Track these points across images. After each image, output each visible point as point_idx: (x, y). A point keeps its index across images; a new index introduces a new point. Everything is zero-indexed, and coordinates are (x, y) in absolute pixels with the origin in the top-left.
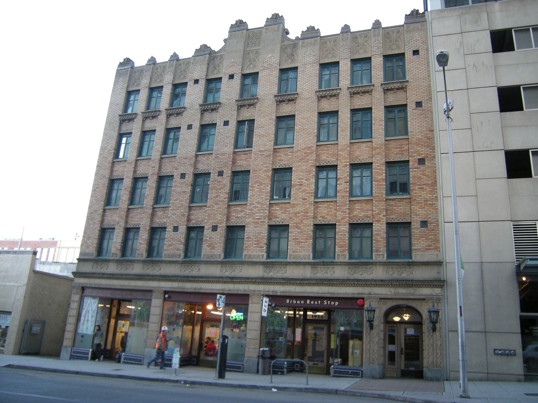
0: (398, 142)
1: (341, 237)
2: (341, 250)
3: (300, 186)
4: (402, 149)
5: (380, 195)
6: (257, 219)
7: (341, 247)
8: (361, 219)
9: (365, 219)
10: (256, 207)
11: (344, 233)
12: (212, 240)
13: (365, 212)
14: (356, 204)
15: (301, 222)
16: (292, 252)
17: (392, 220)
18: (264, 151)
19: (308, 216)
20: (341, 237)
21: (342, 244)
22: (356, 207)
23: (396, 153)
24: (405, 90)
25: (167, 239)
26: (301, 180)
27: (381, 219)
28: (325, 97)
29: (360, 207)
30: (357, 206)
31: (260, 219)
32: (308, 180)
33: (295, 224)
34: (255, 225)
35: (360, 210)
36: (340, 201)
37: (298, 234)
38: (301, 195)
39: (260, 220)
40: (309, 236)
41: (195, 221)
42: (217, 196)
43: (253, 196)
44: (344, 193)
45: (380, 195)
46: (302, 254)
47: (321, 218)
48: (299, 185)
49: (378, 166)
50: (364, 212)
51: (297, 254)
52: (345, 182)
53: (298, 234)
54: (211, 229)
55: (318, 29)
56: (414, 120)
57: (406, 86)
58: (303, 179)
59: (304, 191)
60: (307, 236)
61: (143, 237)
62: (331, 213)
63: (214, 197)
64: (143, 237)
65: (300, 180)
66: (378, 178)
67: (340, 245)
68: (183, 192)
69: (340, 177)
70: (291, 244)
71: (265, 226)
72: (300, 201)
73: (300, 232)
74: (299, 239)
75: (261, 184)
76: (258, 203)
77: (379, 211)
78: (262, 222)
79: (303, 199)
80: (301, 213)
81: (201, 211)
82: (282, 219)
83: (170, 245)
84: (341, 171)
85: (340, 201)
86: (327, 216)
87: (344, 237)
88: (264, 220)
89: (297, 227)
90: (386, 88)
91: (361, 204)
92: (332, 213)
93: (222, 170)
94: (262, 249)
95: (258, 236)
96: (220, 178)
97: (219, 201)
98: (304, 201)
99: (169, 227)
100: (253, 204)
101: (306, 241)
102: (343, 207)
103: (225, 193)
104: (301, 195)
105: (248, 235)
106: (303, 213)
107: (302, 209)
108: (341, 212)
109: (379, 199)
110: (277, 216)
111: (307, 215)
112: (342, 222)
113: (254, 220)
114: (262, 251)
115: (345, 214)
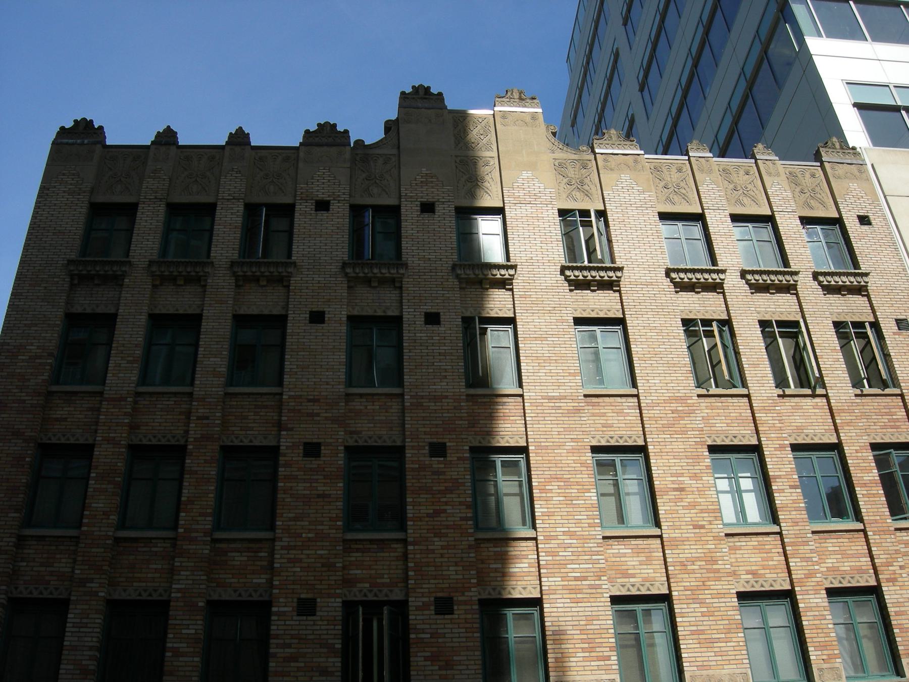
0: (880, 401)
1: (816, 622)
2: (824, 657)
3: (678, 493)
4: (894, 417)
5: (878, 518)
6: (576, 579)
7: (822, 647)
8: (848, 577)
9: (857, 577)
10: (566, 547)
11: (821, 613)
12: (440, 640)
13: (854, 560)
14: (828, 541)
15: (703, 587)
16: (695, 668)
17: (631, 588)
18: (560, 398)
19: (718, 571)
20: (816, 622)
21: (823, 639)
22: (830, 549)
23: (883, 424)
24: (285, 284)
25: (277, 637)
26: (680, 479)
27: (897, 576)
28: (173, 279)
29: (837, 548)
30: (831, 544)
31: (585, 578)
32: (695, 477)
33: (689, 593)
34: (574, 596)
35: (840, 556)
36: (790, 532)
37: (702, 619)
38: (688, 516)
39: (584, 583)
40: (731, 622)
41: (367, 585)
42: (437, 513)
43: (549, 515)
44: (794, 513)
45: (878, 518)
46: (724, 672)
47: (750, 576)
48: (675, 490)
49: (857, 451)
50: (850, 560)
51: (711, 672)
52: (791, 487)
53: (702, 619)
54: (432, 608)
55: (101, 128)
56: (431, 351)
57: (290, 275)
58: (682, 475)
59: (692, 506)
60: (727, 622)
61: (184, 631)
62: (771, 563)
63: (428, 515)
64: (184, 631)
65: (675, 479)
66: (865, 478)
67: (817, 644)
68: (319, 496)
69: (776, 474)
70: (689, 646)
71: (603, 600)
72: (689, 532)
73: (707, 614)
74: (709, 632)
75: (568, 483)
76: (571, 534)
77: (889, 556)
78: (591, 587)
79: (696, 527)
80: (699, 563)
81: (387, 554)
82: (645, 580)
83: (293, 658)
84: (776, 459)
85: (790, 532)
86: (762, 572)
87: (823, 622)
88: (597, 582)
89: (695, 600)
90: (363, 275)
91: (839, 540)
92: (775, 563)
93: (440, 441)
94: (607, 662)
95: (588, 627)
96: (436, 463)
97: (448, 527)
98: (697, 531)
99: (281, 600)
100: (555, 538)
101: (728, 635)
102: (802, 547)
103: (461, 503)
104: (688, 516)
105: (555, 624)
106: (704, 563)
107: (699, 551)
108: (799, 560)
109: (880, 529)
110: (630, 572)
111: (715, 567)
112: (808, 584)
113: (566, 583)
114: (607, 670)
115: (810, 563)
